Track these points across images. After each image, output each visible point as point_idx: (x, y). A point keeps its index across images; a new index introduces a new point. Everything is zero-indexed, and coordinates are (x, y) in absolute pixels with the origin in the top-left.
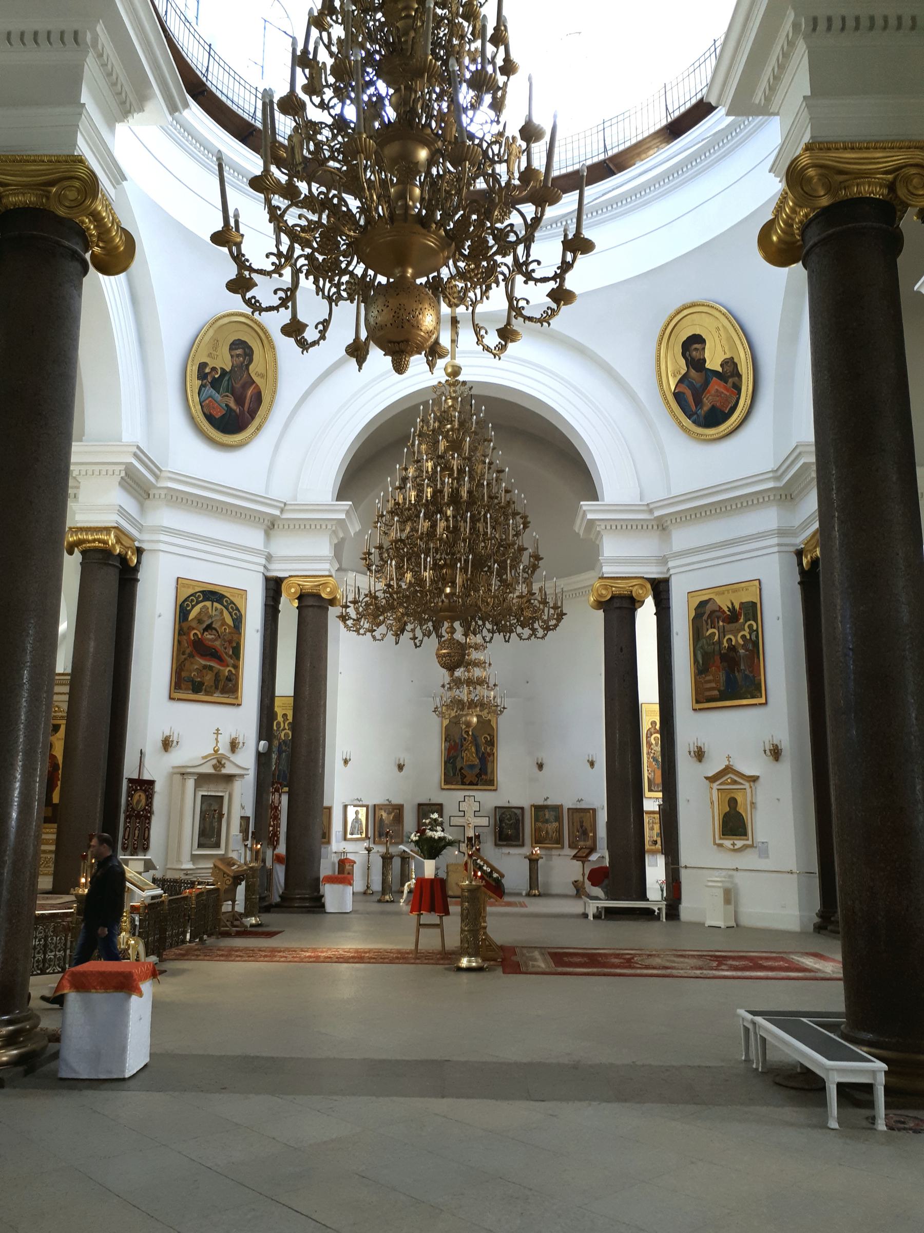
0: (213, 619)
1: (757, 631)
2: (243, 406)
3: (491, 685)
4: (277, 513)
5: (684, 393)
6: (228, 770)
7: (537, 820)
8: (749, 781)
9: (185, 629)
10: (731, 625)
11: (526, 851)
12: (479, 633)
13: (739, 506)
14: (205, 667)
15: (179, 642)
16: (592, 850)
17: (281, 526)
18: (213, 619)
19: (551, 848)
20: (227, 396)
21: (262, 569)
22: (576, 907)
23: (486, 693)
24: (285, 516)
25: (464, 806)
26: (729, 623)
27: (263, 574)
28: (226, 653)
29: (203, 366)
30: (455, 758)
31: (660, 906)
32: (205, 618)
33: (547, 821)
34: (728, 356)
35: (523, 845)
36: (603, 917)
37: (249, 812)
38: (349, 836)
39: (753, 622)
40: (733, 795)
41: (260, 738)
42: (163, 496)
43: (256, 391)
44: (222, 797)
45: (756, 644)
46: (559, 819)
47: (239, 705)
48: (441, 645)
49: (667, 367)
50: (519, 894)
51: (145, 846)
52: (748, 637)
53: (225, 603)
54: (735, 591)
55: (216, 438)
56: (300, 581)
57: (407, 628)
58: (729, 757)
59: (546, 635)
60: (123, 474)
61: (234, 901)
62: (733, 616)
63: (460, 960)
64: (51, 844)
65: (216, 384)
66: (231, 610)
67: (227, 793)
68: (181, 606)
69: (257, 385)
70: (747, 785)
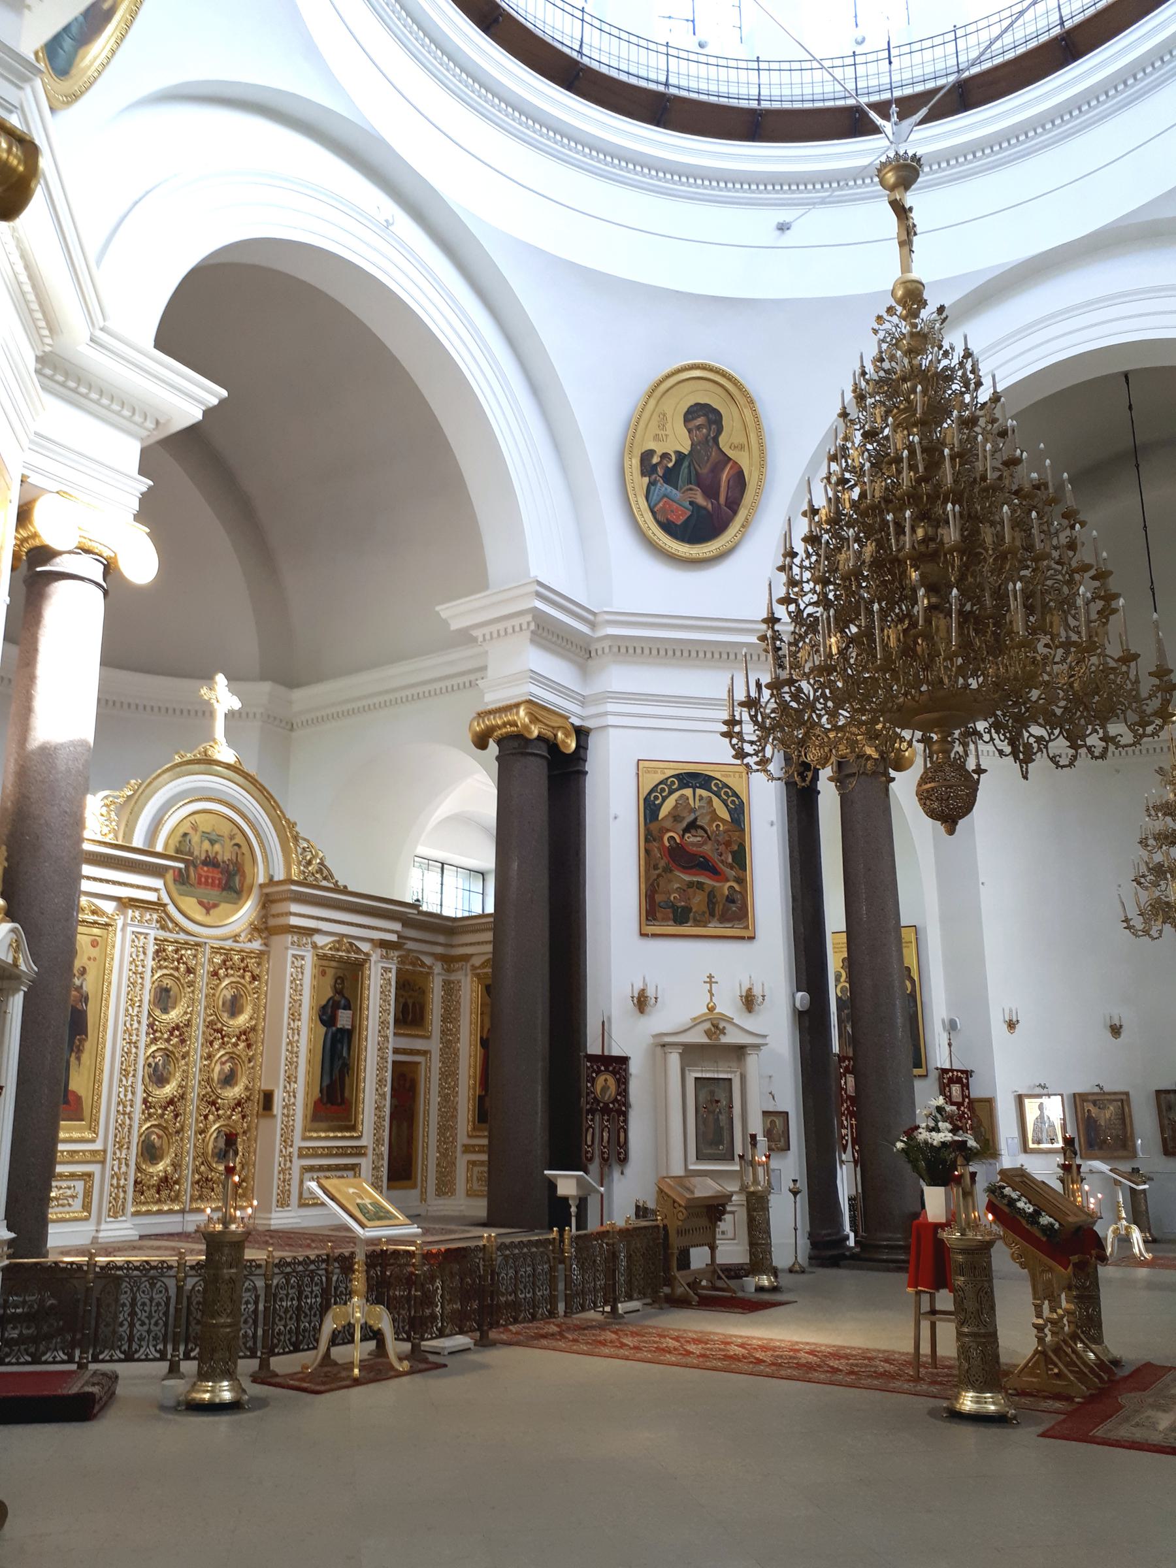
0: (698, 814)
2: (717, 500)
6: (732, 1037)
9: (655, 833)
14: (691, 885)
15: (647, 851)
18: (698, 814)
20: (691, 489)
28: (722, 862)
29: (647, 456)
32: (685, 814)
38: (1031, 1146)
42: (607, 650)
43: (733, 472)
47: (752, 938)
51: (622, 1156)
60: (533, 626)
63: (957, 1397)
64: (479, 1152)
65: (670, 477)
67: (738, 1073)
68: (645, 800)
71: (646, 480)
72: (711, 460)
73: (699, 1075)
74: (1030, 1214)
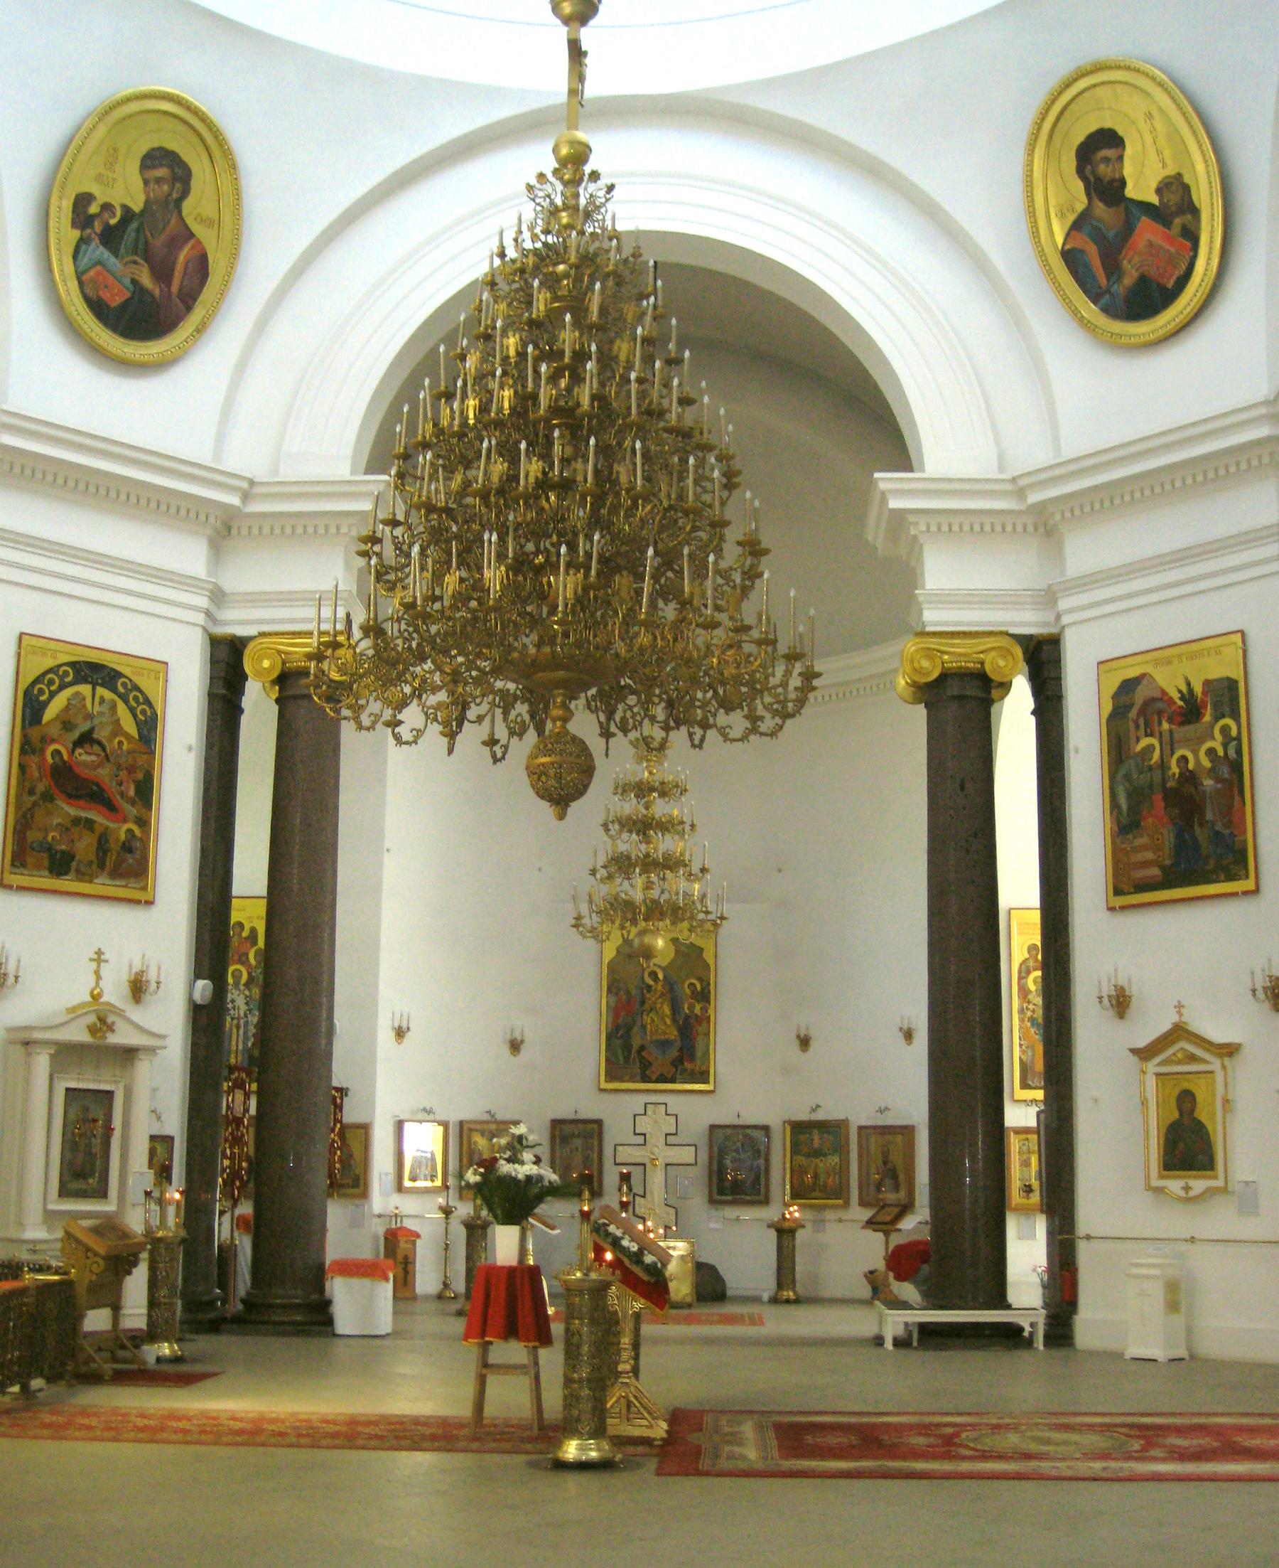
0: (96, 721)
1: (1239, 739)
2: (169, 285)
3: (695, 869)
4: (234, 500)
5: (1082, 252)
6: (122, 1036)
7: (795, 1149)
8: (1221, 1056)
10: (1186, 728)
11: (770, 1213)
12: (635, 727)
13: (1200, 478)
14: (76, 821)
15: (22, 768)
16: (906, 1208)
17: (245, 532)
19: (824, 1207)
20: (135, 262)
21: (200, 618)
22: (860, 1323)
23: (683, 885)
24: (256, 507)
25: (644, 1125)
26: (1182, 724)
27: (205, 630)
28: (122, 794)
29: (83, 200)
30: (629, 1029)
31: (1033, 1320)
32: (79, 720)
33: (817, 1153)
34: (1171, 170)
35: (766, 1201)
36: (915, 1344)
37: (174, 1123)
38: (407, 1183)
39: (1228, 721)
40: (1186, 1085)
41: (198, 975)
44: (110, 1094)
45: (1236, 767)
46: (841, 1148)
47: (150, 903)
48: (543, 748)
49: (1046, 199)
50: (756, 1300)
52: (1221, 753)
53: (121, 689)
54: (1193, 656)
55: (109, 348)
56: (283, 644)
57: (472, 714)
58: (1179, 1006)
59: (781, 727)
61: (116, 1308)
62: (1190, 711)
65: (111, 238)
66: (133, 704)
69: (199, 242)
70: (1215, 1064)
71: (77, 234)
72: (168, 230)
73: (73, 1085)
74: (634, 1253)
